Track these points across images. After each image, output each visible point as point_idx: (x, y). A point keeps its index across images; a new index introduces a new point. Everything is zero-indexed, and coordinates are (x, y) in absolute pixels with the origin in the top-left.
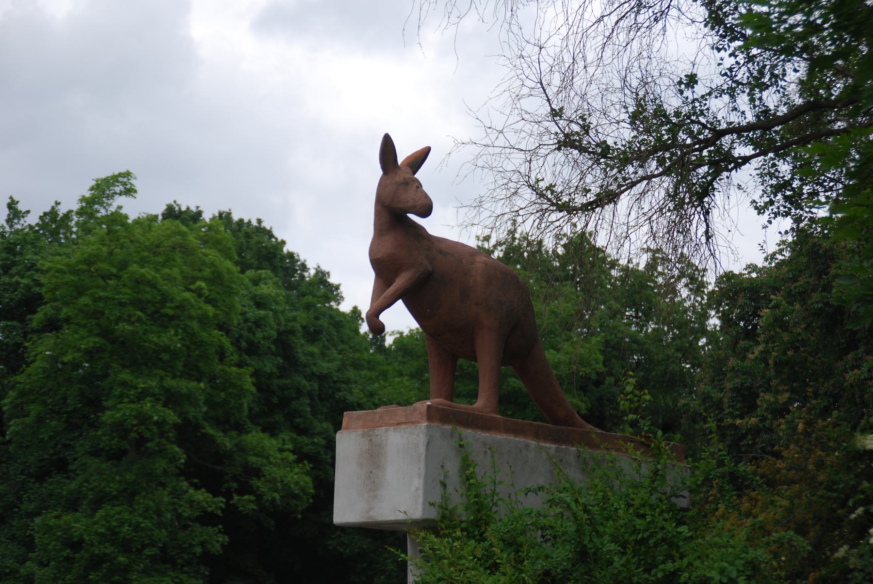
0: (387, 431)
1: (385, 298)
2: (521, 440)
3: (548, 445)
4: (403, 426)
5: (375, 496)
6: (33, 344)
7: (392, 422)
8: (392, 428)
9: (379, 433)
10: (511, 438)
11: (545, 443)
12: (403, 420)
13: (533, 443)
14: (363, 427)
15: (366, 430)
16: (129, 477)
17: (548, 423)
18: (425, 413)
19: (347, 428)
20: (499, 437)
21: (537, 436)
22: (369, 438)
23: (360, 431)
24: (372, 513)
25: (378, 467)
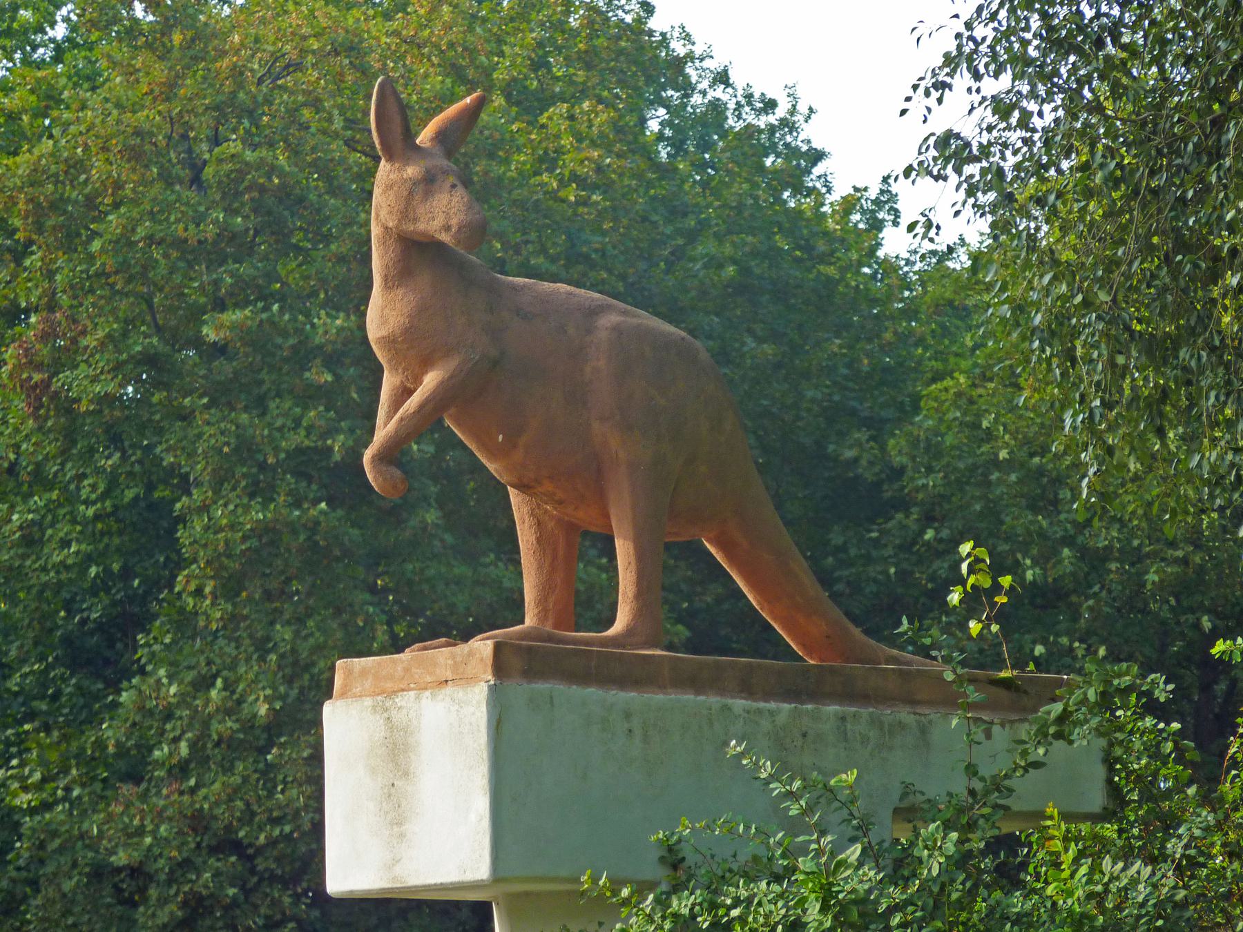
0: (418, 698)
1: (402, 419)
2: (713, 700)
3: (772, 705)
4: (449, 690)
5: (402, 836)
6: (94, 533)
7: (429, 679)
8: (428, 693)
9: (403, 703)
10: (689, 697)
11: (766, 701)
12: (449, 675)
13: (739, 704)
14: (374, 694)
15: (379, 698)
16: (1028, 562)
17: (765, 657)
18: (490, 662)
19: (343, 695)
20: (661, 696)
21: (747, 688)
22: (386, 715)
23: (368, 702)
24: (398, 870)
25: (406, 774)
